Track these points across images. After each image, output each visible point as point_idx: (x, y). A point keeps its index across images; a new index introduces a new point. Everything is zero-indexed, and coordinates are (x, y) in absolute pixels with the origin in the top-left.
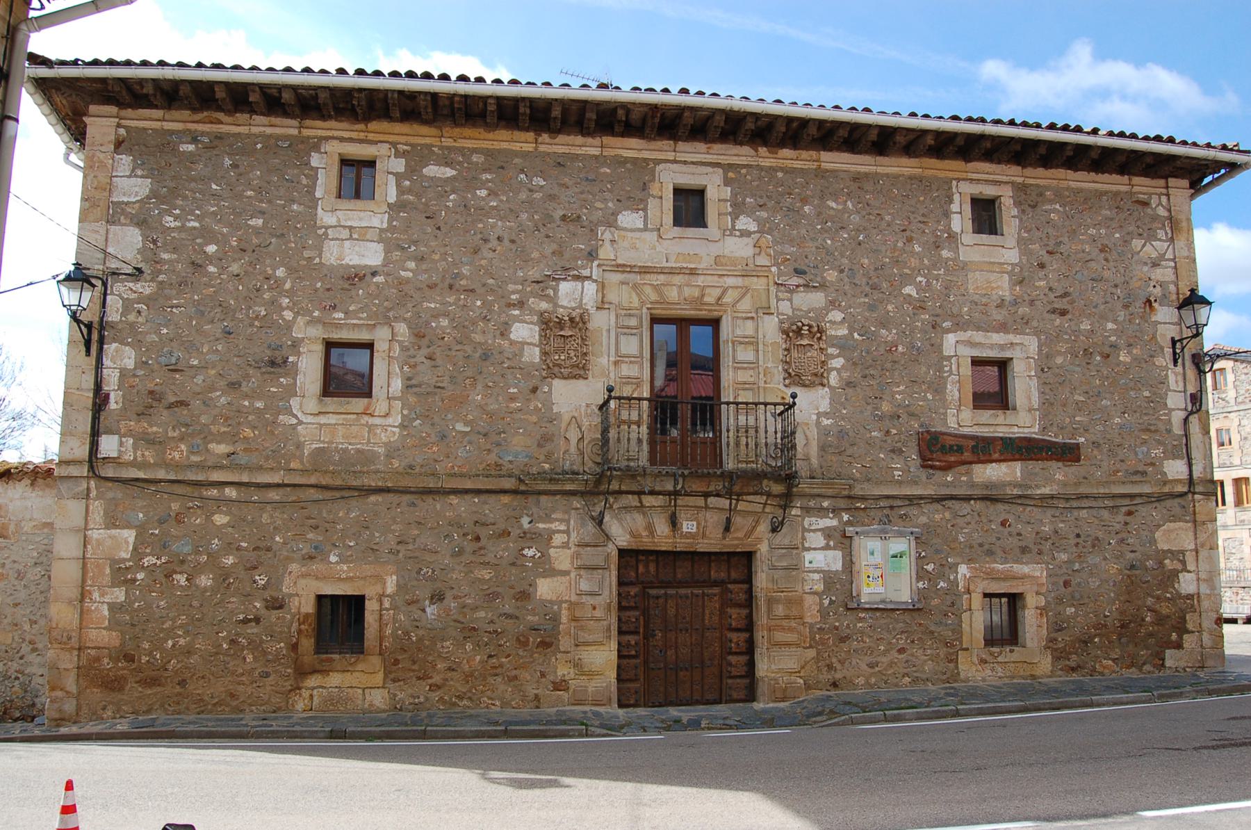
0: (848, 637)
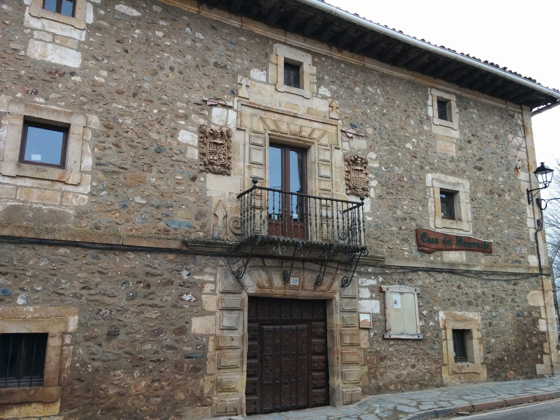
0: (385, 358)
